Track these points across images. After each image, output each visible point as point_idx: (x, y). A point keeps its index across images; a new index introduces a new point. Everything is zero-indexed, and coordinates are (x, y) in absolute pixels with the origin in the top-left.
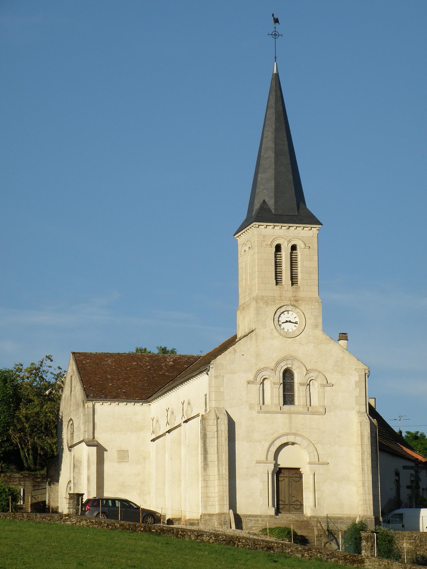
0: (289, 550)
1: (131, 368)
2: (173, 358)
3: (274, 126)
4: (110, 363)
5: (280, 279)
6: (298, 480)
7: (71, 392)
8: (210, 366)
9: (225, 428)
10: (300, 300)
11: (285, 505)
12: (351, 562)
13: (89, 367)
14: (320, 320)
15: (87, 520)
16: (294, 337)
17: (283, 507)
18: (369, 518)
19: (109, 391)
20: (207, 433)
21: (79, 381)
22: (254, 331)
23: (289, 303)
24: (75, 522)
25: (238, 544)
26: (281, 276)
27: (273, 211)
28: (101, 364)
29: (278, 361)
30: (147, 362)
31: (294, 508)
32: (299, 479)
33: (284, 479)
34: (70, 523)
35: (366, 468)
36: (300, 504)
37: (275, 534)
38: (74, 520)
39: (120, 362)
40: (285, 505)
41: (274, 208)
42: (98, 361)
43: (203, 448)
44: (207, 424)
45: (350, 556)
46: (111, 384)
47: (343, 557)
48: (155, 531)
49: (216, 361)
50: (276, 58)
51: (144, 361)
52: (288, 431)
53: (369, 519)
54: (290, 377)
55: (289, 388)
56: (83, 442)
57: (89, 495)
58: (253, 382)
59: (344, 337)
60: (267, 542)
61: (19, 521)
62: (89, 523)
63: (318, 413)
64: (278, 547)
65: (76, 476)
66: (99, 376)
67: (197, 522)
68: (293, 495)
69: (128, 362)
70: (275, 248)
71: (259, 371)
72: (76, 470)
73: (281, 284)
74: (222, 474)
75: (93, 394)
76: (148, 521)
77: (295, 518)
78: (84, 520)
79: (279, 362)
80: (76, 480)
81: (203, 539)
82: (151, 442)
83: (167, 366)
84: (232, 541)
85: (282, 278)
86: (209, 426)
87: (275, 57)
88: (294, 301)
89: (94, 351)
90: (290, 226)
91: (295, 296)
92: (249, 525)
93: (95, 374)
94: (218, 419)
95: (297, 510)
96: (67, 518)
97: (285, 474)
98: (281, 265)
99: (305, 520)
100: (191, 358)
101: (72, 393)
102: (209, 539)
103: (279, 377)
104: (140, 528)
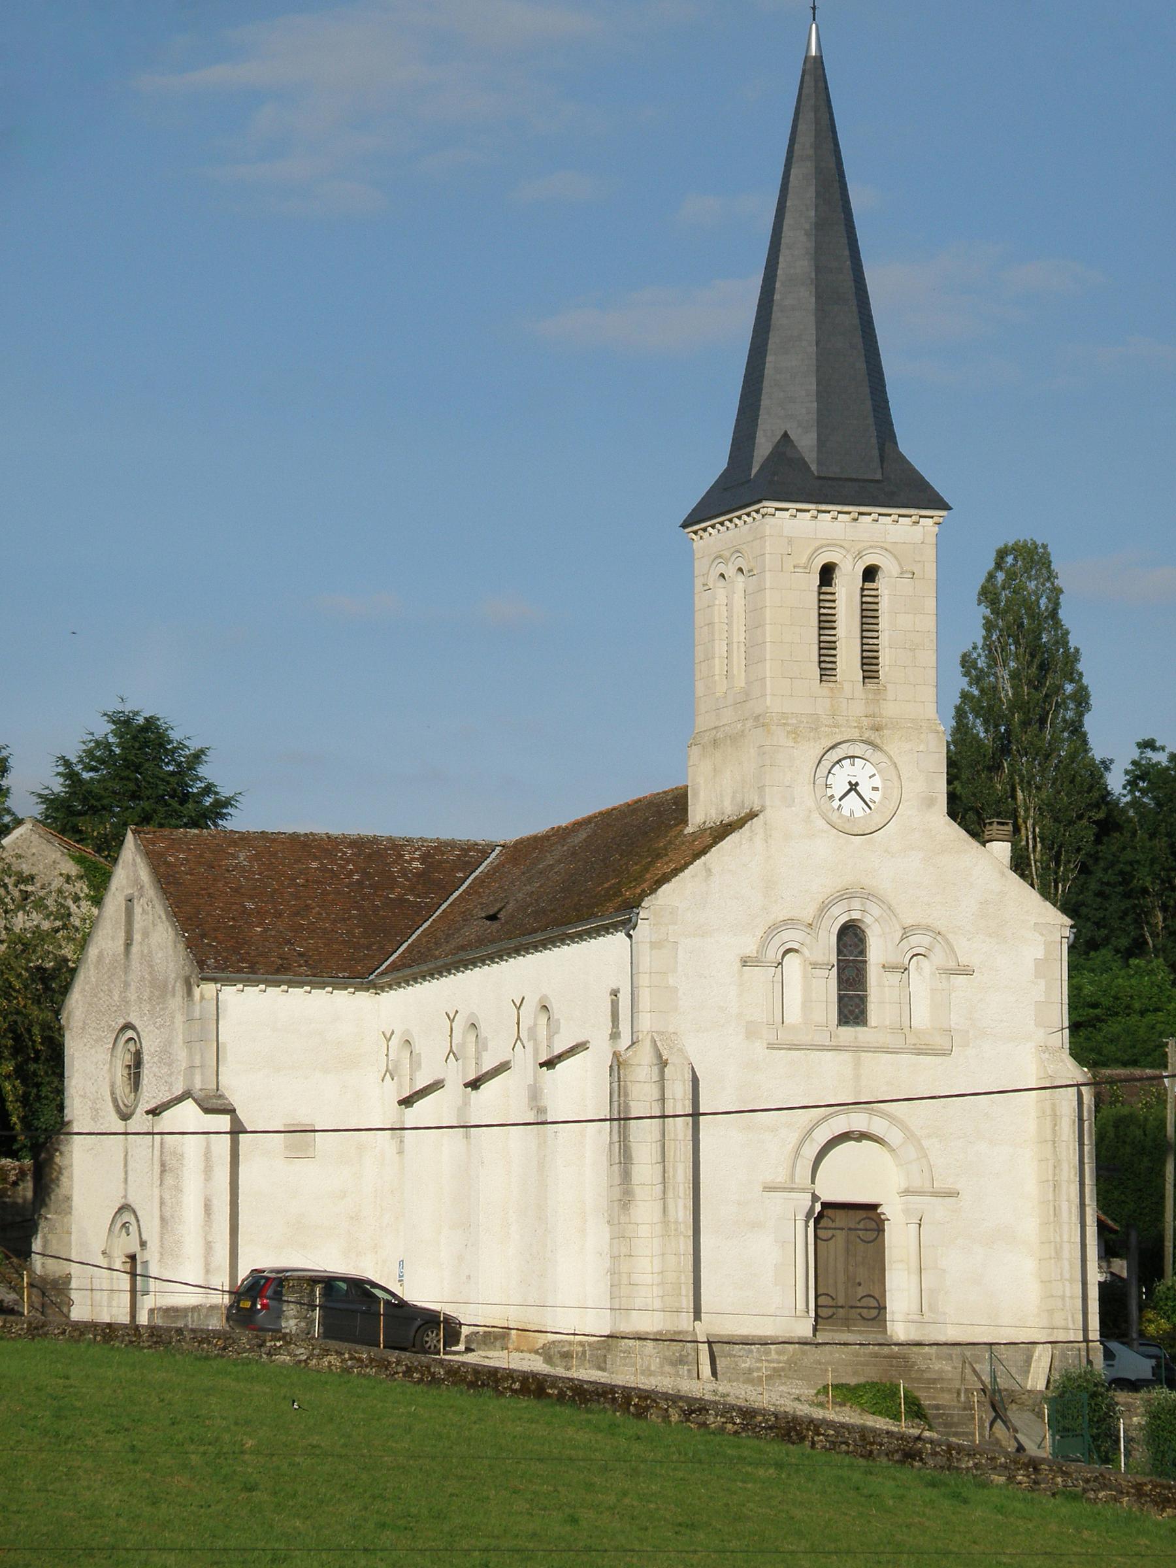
0: (968, 1461)
2: (419, 849)
3: (812, 213)
5: (829, 666)
6: (871, 1239)
7: (128, 945)
8: (638, 914)
9: (685, 1090)
10: (886, 725)
12: (1156, 1502)
13: (187, 874)
15: (344, 1354)
16: (869, 832)
17: (830, 1314)
19: (257, 949)
20: (632, 1104)
21: (164, 917)
22: (761, 816)
23: (855, 734)
25: (813, 1438)
26: (834, 656)
27: (814, 467)
28: (220, 866)
29: (826, 902)
30: (348, 861)
32: (875, 1236)
33: (833, 1236)
34: (288, 1358)
35: (1065, 1206)
36: (877, 1305)
37: (866, 1403)
39: (274, 860)
41: (818, 458)
43: (620, 1145)
45: (1155, 1487)
46: (259, 929)
47: (1132, 1487)
48: (556, 1392)
49: (656, 899)
51: (341, 858)
54: (856, 946)
55: (854, 979)
57: (208, 1254)
58: (757, 961)
60: (902, 1439)
61: (126, 1345)
62: (349, 1363)
63: (932, 1050)
64: (935, 1454)
65: (167, 1197)
66: (221, 905)
67: (580, 1349)
68: (858, 1281)
69: (296, 862)
70: (820, 574)
71: (774, 929)
72: (169, 1180)
73: (833, 677)
74: (676, 1222)
75: (215, 958)
76: (427, 1342)
78: (333, 1353)
79: (829, 903)
84: (796, 1430)
85: (835, 662)
86: (638, 1085)
87: (814, 8)
88: (871, 729)
90: (861, 511)
91: (874, 714)
92: (743, 1365)
93: (209, 895)
94: (665, 1066)
95: (870, 1322)
96: (278, 1344)
97: (837, 1223)
98: (834, 625)
100: (469, 850)
101: (135, 949)
102: (723, 1423)
103: (826, 947)
104: (511, 1384)
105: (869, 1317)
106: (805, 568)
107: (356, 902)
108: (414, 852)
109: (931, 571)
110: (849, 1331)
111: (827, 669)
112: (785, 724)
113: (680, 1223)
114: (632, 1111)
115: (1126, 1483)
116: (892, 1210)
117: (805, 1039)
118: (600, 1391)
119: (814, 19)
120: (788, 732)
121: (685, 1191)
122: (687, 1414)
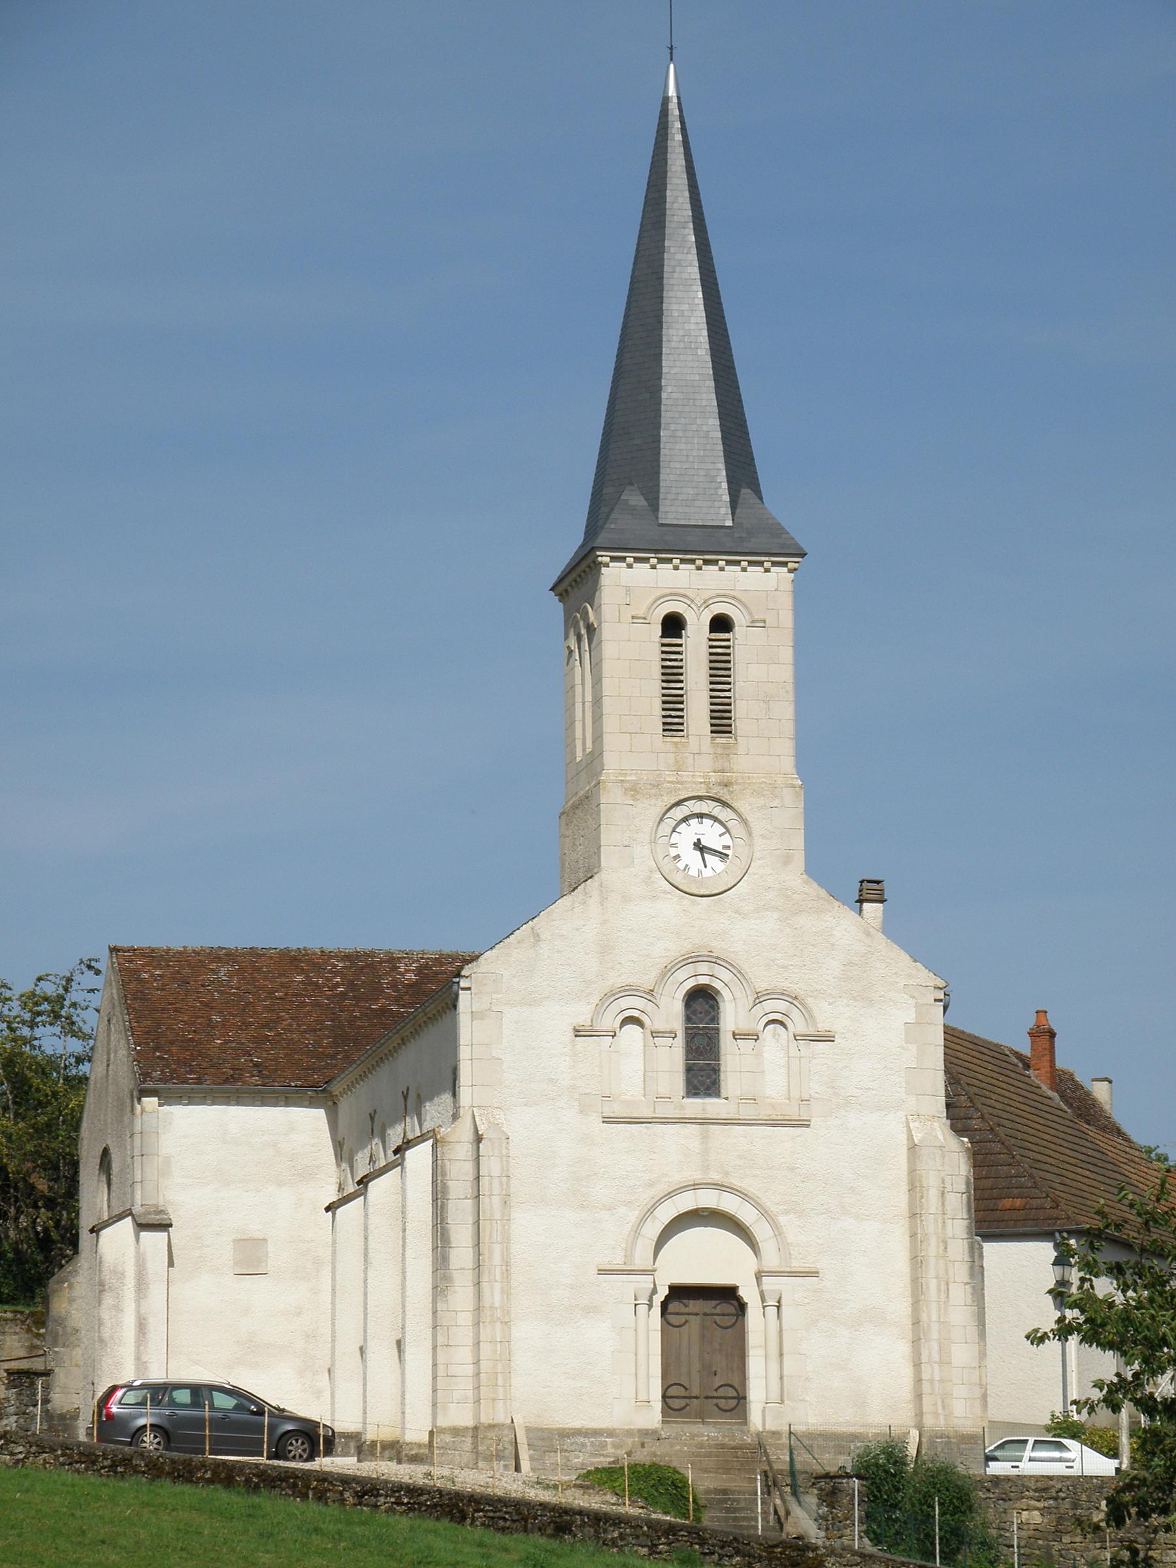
1: (286, 994)
4: (224, 978)
11: (690, 1398)
13: (158, 990)
14: (798, 842)
15: (56, 1451)
17: (683, 1405)
18: (942, 1434)
20: (450, 1183)
24: (21, 1456)
29: (668, 967)
30: (336, 974)
31: (716, 1408)
32: (733, 1321)
33: (686, 1321)
34: (8, 1457)
36: (735, 1394)
38: (21, 1449)
40: (690, 1398)
42: (187, 971)
44: (451, 1158)
46: (219, 1042)
50: (674, 51)
51: (330, 971)
52: (698, 1176)
53: (941, 1437)
56: (127, 1216)
59: (872, 892)
62: (61, 1459)
63: (789, 1120)
69: (280, 975)
71: (613, 995)
75: (162, 1071)
77: (718, 1437)
79: (672, 967)
80: (107, 1329)
81: (376, 1503)
82: (327, 1212)
83: (396, 986)
86: (458, 1163)
87: (671, 48)
89: (177, 945)
99: (750, 1444)
105: (727, 1408)
106: (645, 618)
107: (333, 1014)
108: (411, 964)
109: (787, 618)
110: (703, 1423)
111: (673, 723)
112: (622, 781)
113: (496, 1309)
114: (451, 1194)
115: (758, 1547)
116: (748, 1293)
117: (647, 1112)
118: (283, 1475)
119: (671, 60)
120: (626, 789)
121: (503, 1273)
122: (360, 1496)
